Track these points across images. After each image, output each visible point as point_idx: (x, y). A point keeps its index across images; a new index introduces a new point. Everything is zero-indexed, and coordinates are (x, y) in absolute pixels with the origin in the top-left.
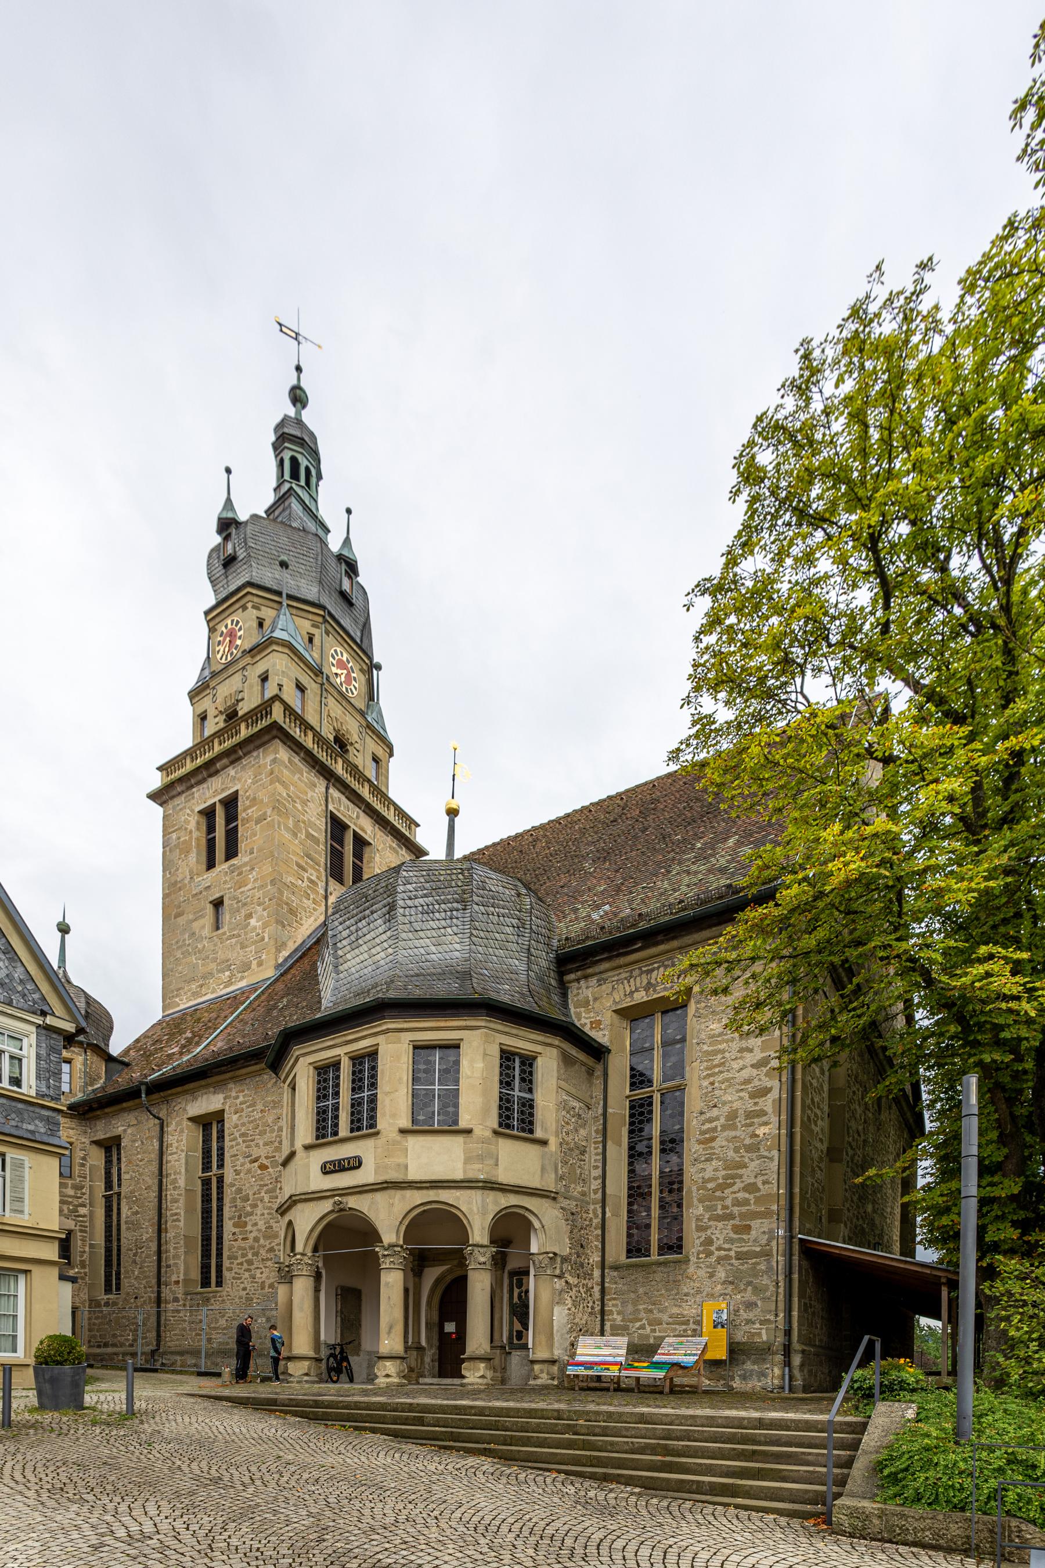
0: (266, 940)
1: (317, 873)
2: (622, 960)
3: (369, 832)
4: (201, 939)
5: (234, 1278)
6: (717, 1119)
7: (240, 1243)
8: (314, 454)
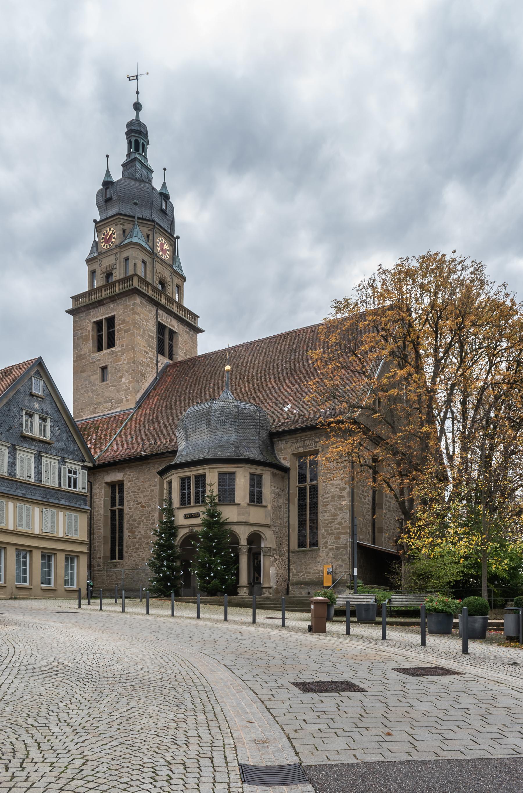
0: (131, 389)
1: (152, 353)
2: (294, 436)
3: (176, 327)
4: (95, 385)
5: (129, 556)
6: (328, 498)
7: (132, 540)
8: (146, 136)
